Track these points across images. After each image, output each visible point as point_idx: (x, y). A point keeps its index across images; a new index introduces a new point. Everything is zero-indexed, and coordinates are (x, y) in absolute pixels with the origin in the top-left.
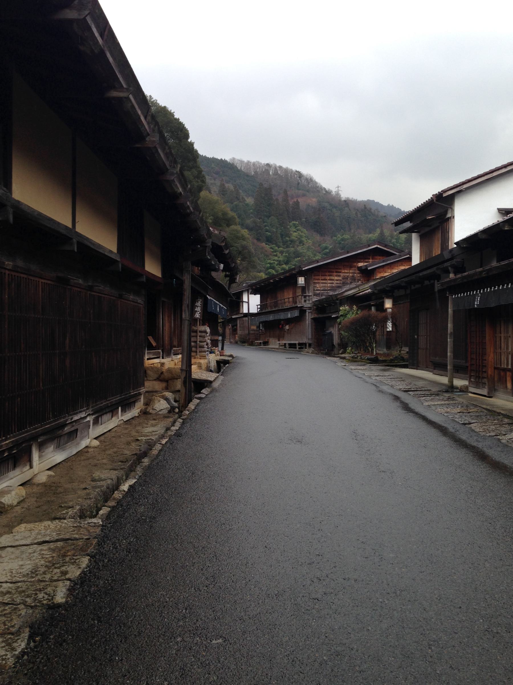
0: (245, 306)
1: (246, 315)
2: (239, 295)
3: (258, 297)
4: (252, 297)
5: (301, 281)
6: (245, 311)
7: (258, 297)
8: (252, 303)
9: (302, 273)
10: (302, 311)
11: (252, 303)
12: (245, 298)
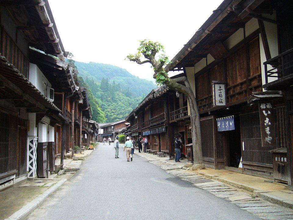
1: (99, 134)
8: (101, 131)
10: (113, 134)
11: (101, 131)
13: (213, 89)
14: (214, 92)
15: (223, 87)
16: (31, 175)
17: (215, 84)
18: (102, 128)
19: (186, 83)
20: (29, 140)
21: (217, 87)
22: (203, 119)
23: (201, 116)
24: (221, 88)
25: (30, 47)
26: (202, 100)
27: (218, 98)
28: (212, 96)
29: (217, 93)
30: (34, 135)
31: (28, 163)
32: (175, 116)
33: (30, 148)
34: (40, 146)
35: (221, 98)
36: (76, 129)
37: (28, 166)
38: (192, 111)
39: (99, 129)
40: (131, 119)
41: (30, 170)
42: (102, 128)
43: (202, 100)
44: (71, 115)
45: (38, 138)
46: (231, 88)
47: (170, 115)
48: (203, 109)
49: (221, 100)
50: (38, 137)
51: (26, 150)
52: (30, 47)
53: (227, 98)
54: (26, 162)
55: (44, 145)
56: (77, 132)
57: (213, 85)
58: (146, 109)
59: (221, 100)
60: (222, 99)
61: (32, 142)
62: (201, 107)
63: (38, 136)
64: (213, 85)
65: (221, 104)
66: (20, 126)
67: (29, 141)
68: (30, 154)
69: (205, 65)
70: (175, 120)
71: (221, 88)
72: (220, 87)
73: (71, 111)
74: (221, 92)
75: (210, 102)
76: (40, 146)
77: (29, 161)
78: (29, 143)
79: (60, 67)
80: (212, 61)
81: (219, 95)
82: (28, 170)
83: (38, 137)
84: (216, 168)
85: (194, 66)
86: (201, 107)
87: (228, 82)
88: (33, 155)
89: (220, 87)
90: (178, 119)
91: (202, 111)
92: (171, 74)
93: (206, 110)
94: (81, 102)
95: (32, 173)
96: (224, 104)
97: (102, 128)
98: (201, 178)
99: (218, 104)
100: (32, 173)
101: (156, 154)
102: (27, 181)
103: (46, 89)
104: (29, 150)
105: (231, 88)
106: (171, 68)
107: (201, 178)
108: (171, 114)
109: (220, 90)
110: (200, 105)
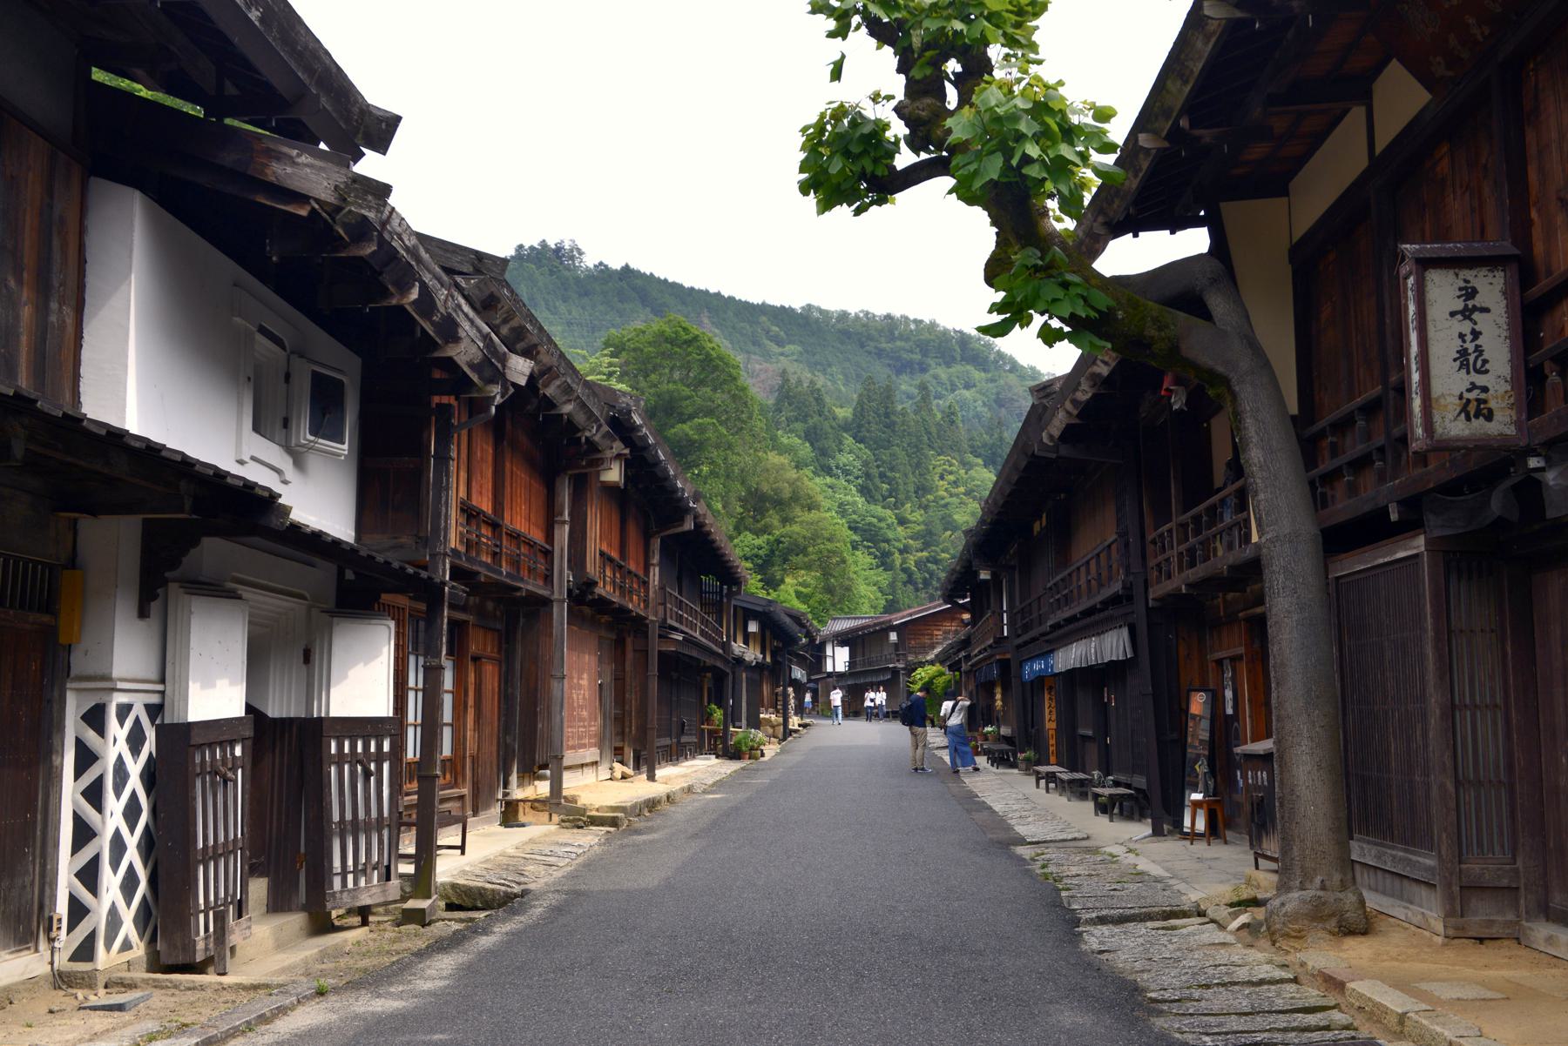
0: (829, 662)
1: (830, 675)
2: (821, 648)
3: (846, 650)
4: (838, 649)
5: (893, 637)
6: (829, 669)
7: (846, 650)
9: (893, 628)
12: (829, 651)
14: (1414, 337)
15: (1491, 288)
16: (85, 951)
17: (1426, 264)
18: (843, 639)
19: (1218, 304)
20: (78, 707)
21: (1443, 290)
22: (1354, 564)
23: (1338, 539)
24: (1478, 301)
25: (98, 75)
26: (1343, 425)
27: (1449, 382)
28: (1402, 390)
29: (1445, 338)
30: (115, 674)
31: (66, 865)
33: (84, 833)
34: (178, 753)
35: (1480, 380)
36: (629, 640)
38: (1277, 521)
40: (961, 583)
41: (78, 911)
42: (842, 644)
43: (1343, 425)
44: (548, 554)
45: (162, 693)
47: (1150, 548)
48: (1353, 490)
49: (1473, 395)
50: (160, 687)
51: (55, 777)
52: (98, 75)
53: (1530, 383)
55: (196, 740)
56: (630, 655)
57: (1411, 281)
58: (1037, 527)
59: (1473, 395)
60: (1485, 389)
61: (96, 718)
62: (1335, 474)
63: (163, 681)
64: (1411, 281)
65: (1479, 426)
66: (738, 647)
67: (73, 708)
68: (83, 801)
69: (1363, 163)
70: (1178, 582)
71: (1478, 301)
72: (1470, 293)
73: (550, 537)
74: (1476, 334)
75: (1396, 432)
76: (178, 753)
81: (1463, 353)
82: (62, 908)
83: (160, 687)
84: (1451, 932)
85: (1284, 192)
86: (1335, 474)
87: (1539, 248)
89: (1470, 293)
90: (1199, 571)
91: (1344, 507)
92: (1131, 255)
93: (1379, 492)
94: (613, 474)
95: (92, 936)
96: (1502, 424)
98: (1312, 1019)
99: (1454, 427)
101: (1083, 796)
102: (59, 999)
103: (288, 377)
107: (1312, 1019)
108: (1154, 542)
109: (1467, 313)
110: (1326, 465)
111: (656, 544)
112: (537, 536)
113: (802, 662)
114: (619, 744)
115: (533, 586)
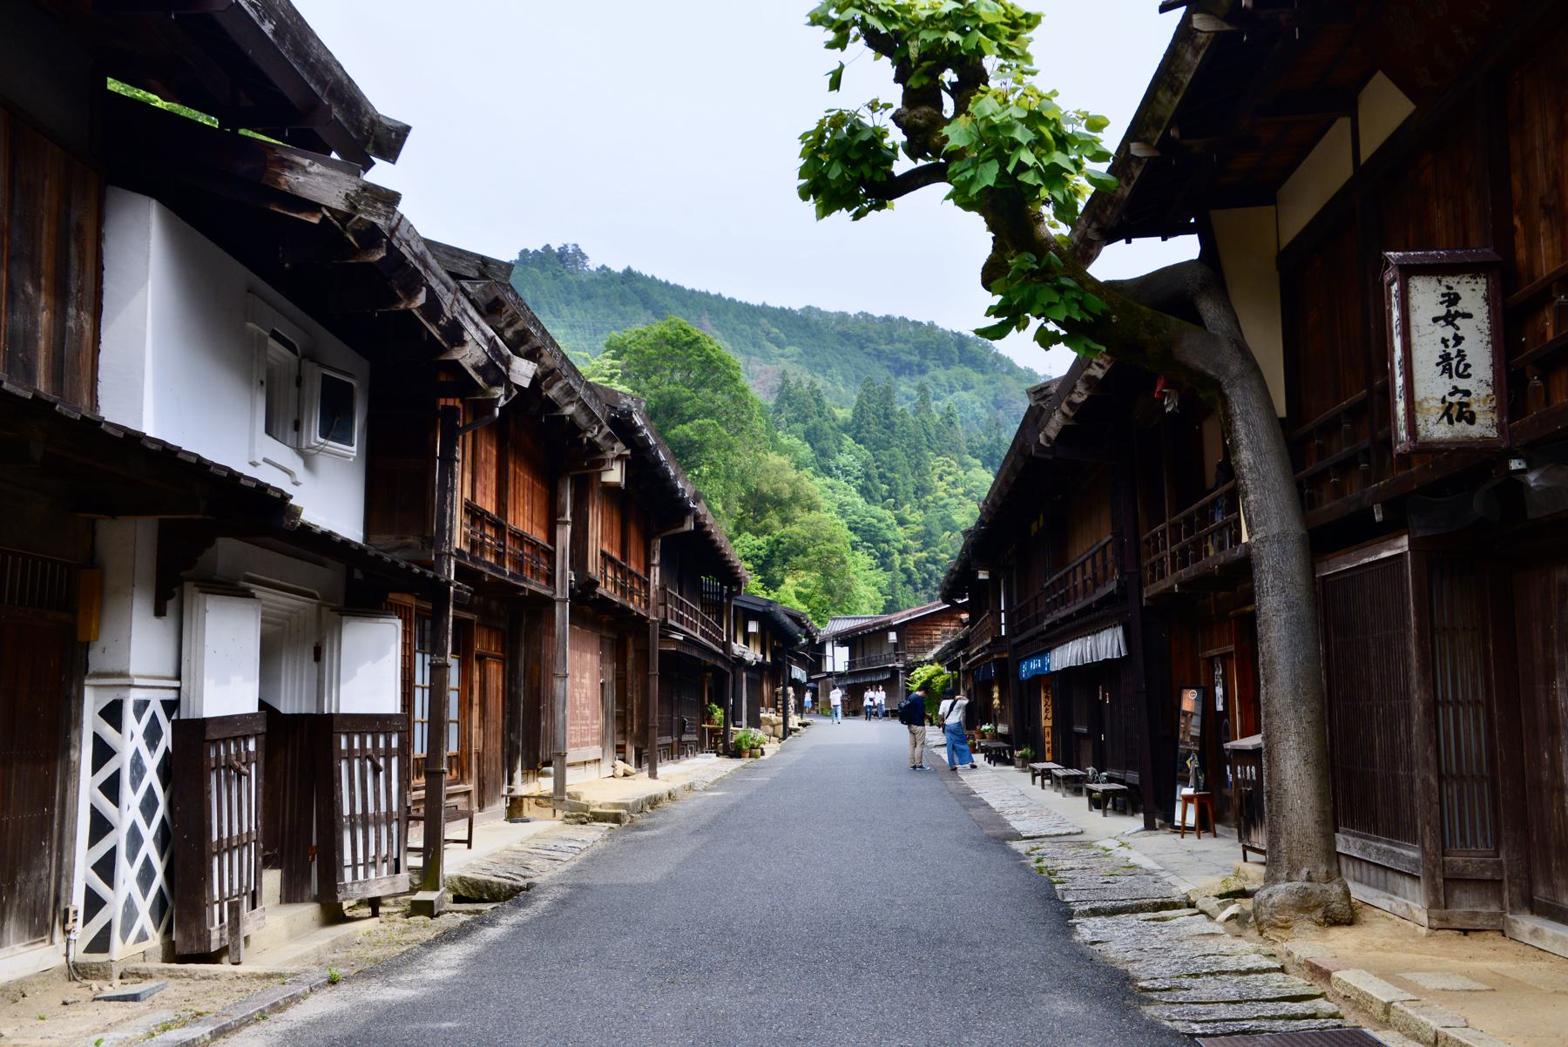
0: (829, 661)
1: (830, 675)
5: (893, 637)
6: (829, 668)
8: (838, 659)
9: (892, 628)
11: (838, 659)
13: (1396, 314)
15: (1473, 295)
17: (1408, 272)
18: (842, 639)
19: (1209, 310)
20: (96, 703)
21: (1426, 297)
24: (1461, 307)
27: (1432, 386)
29: (1428, 343)
31: (83, 858)
32: (1173, 555)
33: (100, 826)
35: (1463, 384)
37: (82, 874)
39: (829, 647)
42: (842, 643)
44: (551, 555)
45: (178, 689)
46: (1543, 297)
49: (1455, 399)
50: (176, 684)
51: (71, 771)
54: (60, 849)
55: (211, 735)
56: (631, 656)
57: (1395, 287)
59: (1455, 399)
60: (1467, 393)
61: (113, 714)
63: (178, 677)
64: (1395, 287)
66: (738, 647)
70: (1170, 581)
71: (1461, 307)
72: (1452, 299)
77: (91, 845)
78: (91, 721)
79: (314, 207)
80: (1405, 115)
81: (1446, 358)
82: (78, 901)
84: (1435, 923)
87: (1522, 255)
88: (116, 802)
89: (1452, 299)
91: (1330, 507)
92: (1125, 261)
94: (614, 475)
95: (108, 928)
96: (1484, 427)
97: (842, 639)
98: (1299, 1008)
99: (1436, 429)
100: (108, 928)
101: (1078, 792)
102: (74, 990)
104: (94, 772)
105: (1543, 297)
106: (1119, 216)
107: (1299, 1008)
109: (1449, 319)
111: (657, 544)
112: (539, 536)
113: (802, 662)
114: (621, 742)
115: (536, 586)
